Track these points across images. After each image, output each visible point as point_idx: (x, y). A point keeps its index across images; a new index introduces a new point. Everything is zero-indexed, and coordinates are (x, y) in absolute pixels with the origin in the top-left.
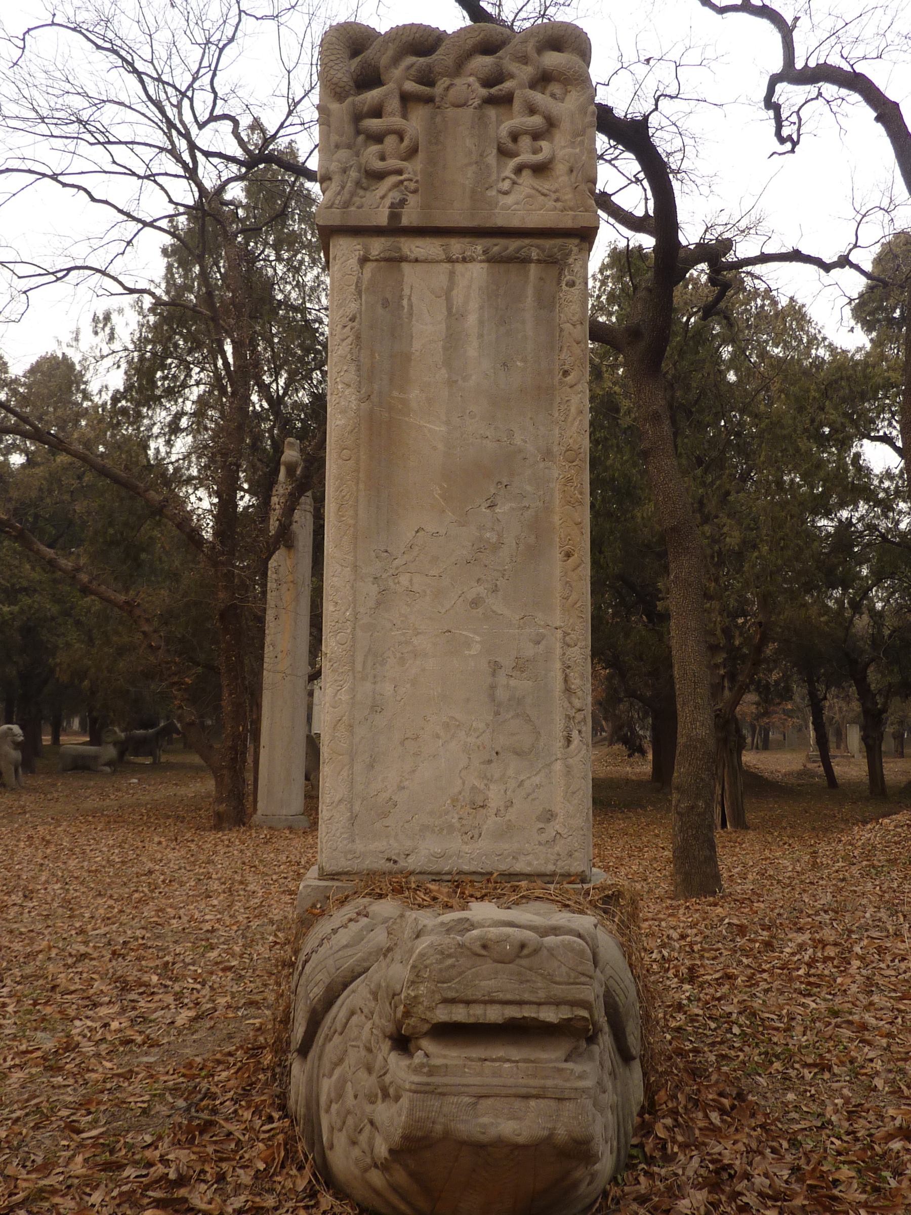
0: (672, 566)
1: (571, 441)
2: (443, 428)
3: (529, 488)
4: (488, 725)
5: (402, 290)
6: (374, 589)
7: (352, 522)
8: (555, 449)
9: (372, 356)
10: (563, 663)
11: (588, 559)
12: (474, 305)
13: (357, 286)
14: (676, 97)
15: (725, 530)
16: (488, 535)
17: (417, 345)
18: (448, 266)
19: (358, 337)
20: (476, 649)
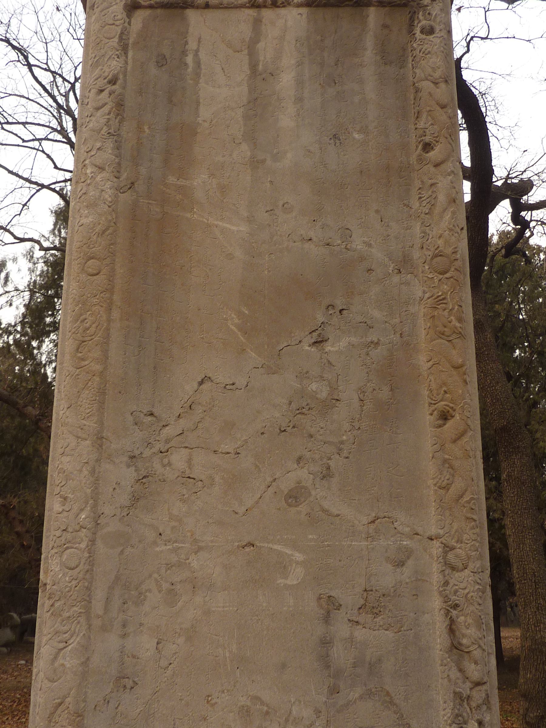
0: (504, 465)
1: (440, 242)
2: (244, 228)
3: (376, 314)
4: (318, 712)
5: (186, 43)
6: (128, 475)
7: (98, 367)
8: (416, 254)
9: (140, 128)
10: (446, 599)
11: (476, 423)
12: (289, 60)
13: (121, 38)
14: (486, 38)
15: (538, 435)
16: (314, 386)
17: (205, 113)
18: (252, 12)
19: (120, 105)
20: (296, 575)
